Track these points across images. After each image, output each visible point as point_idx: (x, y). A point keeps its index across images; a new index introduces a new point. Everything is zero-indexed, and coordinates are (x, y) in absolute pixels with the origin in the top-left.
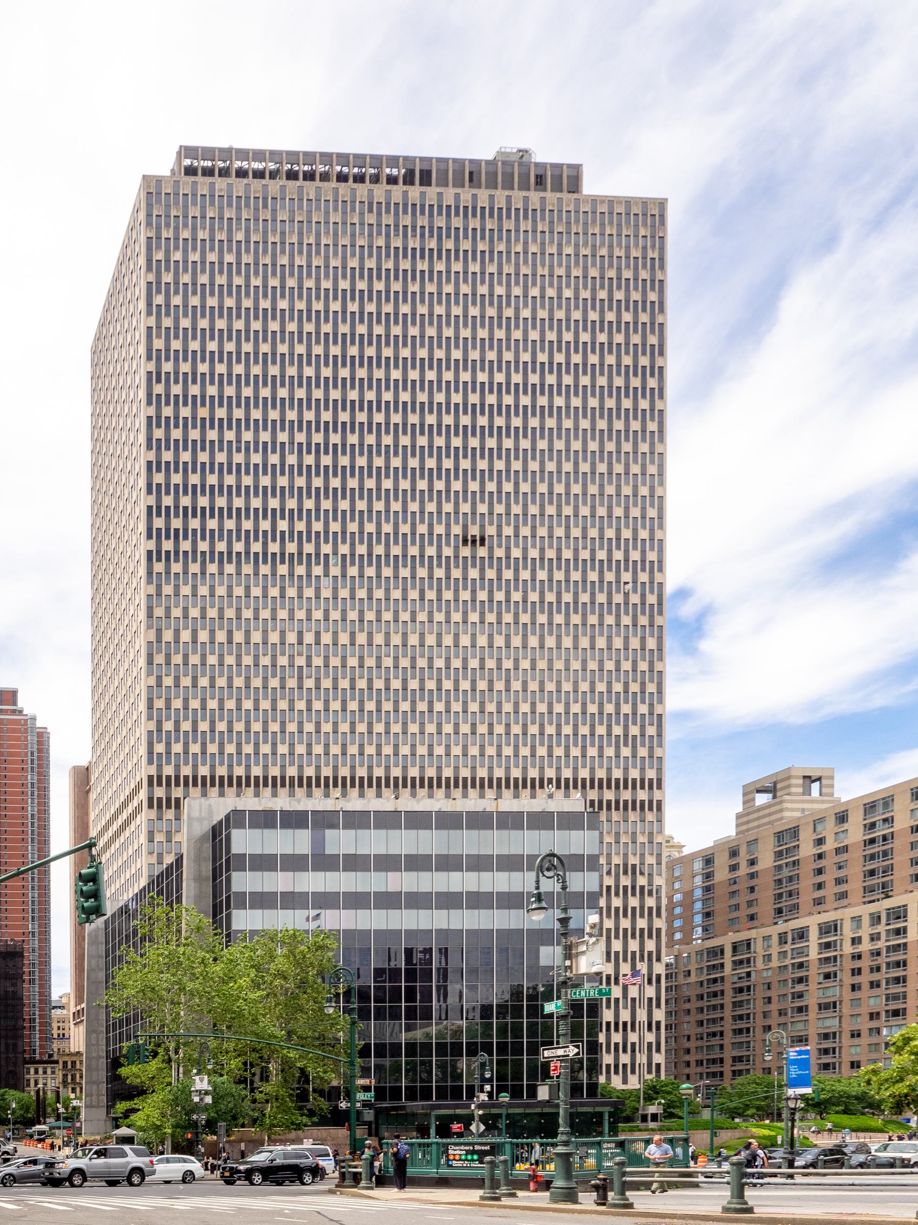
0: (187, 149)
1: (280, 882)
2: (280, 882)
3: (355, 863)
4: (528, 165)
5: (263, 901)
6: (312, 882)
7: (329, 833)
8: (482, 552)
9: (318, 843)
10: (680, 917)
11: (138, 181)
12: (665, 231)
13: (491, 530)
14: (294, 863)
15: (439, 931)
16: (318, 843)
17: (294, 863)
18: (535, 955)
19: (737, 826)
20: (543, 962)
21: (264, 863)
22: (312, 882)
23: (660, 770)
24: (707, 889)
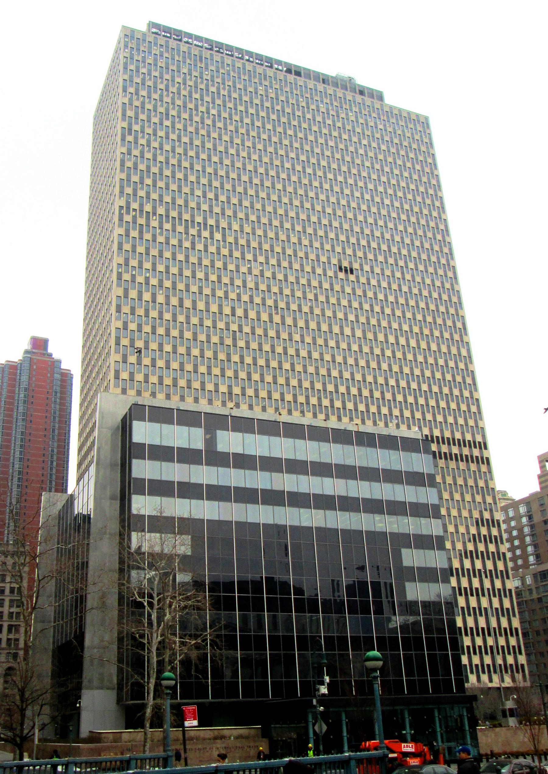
0: (153, 23)
1: (175, 472)
2: (175, 472)
3: (243, 461)
4: (355, 85)
5: (161, 488)
6: (204, 475)
7: (219, 433)
8: (352, 278)
9: (211, 442)
10: (516, 538)
11: (119, 28)
12: (430, 131)
13: (356, 266)
14: (188, 456)
15: (318, 529)
16: (211, 442)
17: (188, 456)
18: (398, 557)
19: (540, 483)
20: (134, 545)
21: (162, 453)
22: (204, 475)
23: (484, 436)
24: (532, 527)
